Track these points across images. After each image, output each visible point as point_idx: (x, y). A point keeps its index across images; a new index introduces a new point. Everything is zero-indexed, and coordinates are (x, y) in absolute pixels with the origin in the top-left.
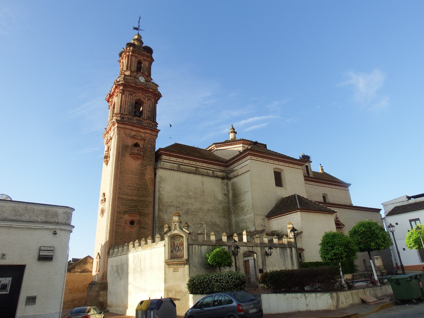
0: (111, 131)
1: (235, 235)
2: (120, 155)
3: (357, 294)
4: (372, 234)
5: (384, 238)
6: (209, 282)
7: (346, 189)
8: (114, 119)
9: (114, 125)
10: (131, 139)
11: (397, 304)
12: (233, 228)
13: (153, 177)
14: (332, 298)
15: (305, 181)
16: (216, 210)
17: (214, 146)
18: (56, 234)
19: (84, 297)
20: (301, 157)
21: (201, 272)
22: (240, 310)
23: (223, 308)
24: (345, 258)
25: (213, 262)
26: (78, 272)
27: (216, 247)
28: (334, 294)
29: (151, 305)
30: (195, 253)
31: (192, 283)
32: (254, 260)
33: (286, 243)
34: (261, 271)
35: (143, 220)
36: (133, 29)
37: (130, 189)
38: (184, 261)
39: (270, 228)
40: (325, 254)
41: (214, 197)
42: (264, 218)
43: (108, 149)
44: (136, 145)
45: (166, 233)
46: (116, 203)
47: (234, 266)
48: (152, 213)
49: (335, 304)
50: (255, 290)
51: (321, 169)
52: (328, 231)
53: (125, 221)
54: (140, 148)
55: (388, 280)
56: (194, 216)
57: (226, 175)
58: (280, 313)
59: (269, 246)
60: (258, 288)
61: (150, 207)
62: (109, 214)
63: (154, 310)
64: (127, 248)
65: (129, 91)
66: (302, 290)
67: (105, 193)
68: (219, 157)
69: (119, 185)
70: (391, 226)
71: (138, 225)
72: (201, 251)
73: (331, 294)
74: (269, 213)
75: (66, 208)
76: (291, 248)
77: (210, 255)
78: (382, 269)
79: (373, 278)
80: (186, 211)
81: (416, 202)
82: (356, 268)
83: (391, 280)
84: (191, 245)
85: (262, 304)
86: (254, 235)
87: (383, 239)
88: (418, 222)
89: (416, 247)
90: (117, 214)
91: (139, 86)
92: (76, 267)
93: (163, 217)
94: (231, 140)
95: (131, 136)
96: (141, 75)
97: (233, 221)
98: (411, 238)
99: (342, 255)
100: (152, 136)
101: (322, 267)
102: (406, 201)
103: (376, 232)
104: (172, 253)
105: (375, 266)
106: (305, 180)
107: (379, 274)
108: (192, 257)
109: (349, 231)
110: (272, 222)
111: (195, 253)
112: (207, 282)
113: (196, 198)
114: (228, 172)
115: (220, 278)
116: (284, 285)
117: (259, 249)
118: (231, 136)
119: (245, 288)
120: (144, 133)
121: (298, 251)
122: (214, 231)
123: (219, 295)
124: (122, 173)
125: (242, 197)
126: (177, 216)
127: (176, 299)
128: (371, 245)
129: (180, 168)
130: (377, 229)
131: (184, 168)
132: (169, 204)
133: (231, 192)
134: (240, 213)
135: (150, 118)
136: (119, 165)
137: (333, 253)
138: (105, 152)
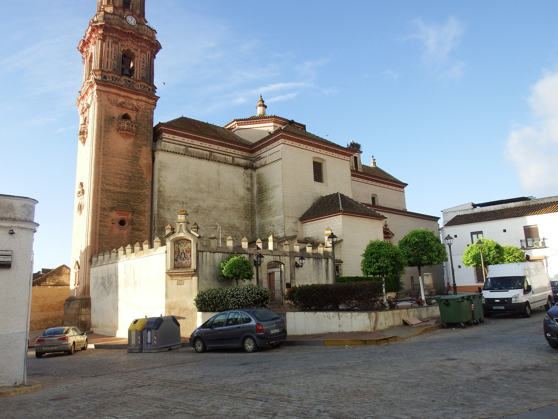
0: (87, 95)
1: (259, 240)
2: (102, 130)
3: (400, 314)
4: (426, 246)
5: (439, 251)
6: (222, 297)
7: (402, 190)
8: (91, 78)
9: (92, 86)
10: (118, 108)
11: (442, 327)
12: (257, 232)
13: (151, 162)
14: (370, 318)
15: (352, 177)
16: (235, 208)
17: (235, 124)
18: (13, 233)
19: (60, 316)
20: (349, 145)
21: (212, 285)
22: (259, 329)
23: (239, 328)
24: (391, 272)
25: (228, 274)
26: (51, 285)
27: (234, 255)
28: (373, 314)
29: (148, 324)
30: (206, 262)
31: (201, 298)
32: (281, 272)
33: (322, 252)
34: (288, 285)
35: (137, 219)
37: (119, 178)
38: (191, 272)
39: (304, 234)
40: (367, 268)
41: (234, 191)
42: (297, 221)
43: (85, 121)
44: (126, 117)
45: (168, 236)
46: (99, 197)
47: (255, 279)
48: (150, 210)
49: (373, 325)
50: (280, 307)
51: (373, 162)
52: (374, 239)
53: (113, 220)
54: (131, 122)
55: (437, 300)
56: (205, 216)
57: (250, 163)
58: (308, 334)
59: (301, 256)
60: (283, 305)
61: (147, 202)
62: (90, 210)
63: (152, 330)
64: (115, 255)
66: (336, 309)
67: (82, 183)
68: (241, 139)
69: (102, 172)
70: (449, 237)
71: (130, 226)
72: (214, 259)
73: (370, 314)
74: (303, 216)
75: (25, 199)
76: (328, 259)
77: (225, 264)
78: (431, 287)
79: (420, 297)
80: (195, 209)
81: (482, 212)
82: (402, 286)
83: (441, 300)
84: (200, 251)
85: (286, 324)
86: (282, 241)
87: (437, 252)
88: (480, 235)
89: (473, 264)
90: (101, 210)
91: (128, 30)
92: (48, 279)
93: (164, 216)
94: (259, 116)
95: (118, 103)
96: (130, 13)
97: (257, 224)
98: (470, 254)
99: (387, 269)
100: (148, 104)
101: (363, 282)
102: (470, 209)
103: (431, 244)
104: (176, 262)
105: (423, 284)
106: (352, 175)
107: (427, 293)
108: (202, 266)
109: (399, 241)
110: (307, 227)
111: (206, 262)
112: (220, 298)
113: (209, 192)
114: (253, 159)
115: (237, 293)
116: (315, 301)
117: (288, 259)
118: (259, 111)
119: (268, 305)
120: (136, 100)
121: (336, 263)
122: (232, 235)
123: (234, 313)
124: (106, 156)
125: (270, 193)
126: (183, 214)
127: (180, 318)
128: (422, 258)
129: (187, 151)
130: (433, 240)
131: (194, 151)
132: (172, 199)
133: (256, 186)
134: (267, 213)
135: (144, 78)
136: (102, 144)
137: (377, 266)
138: (80, 125)
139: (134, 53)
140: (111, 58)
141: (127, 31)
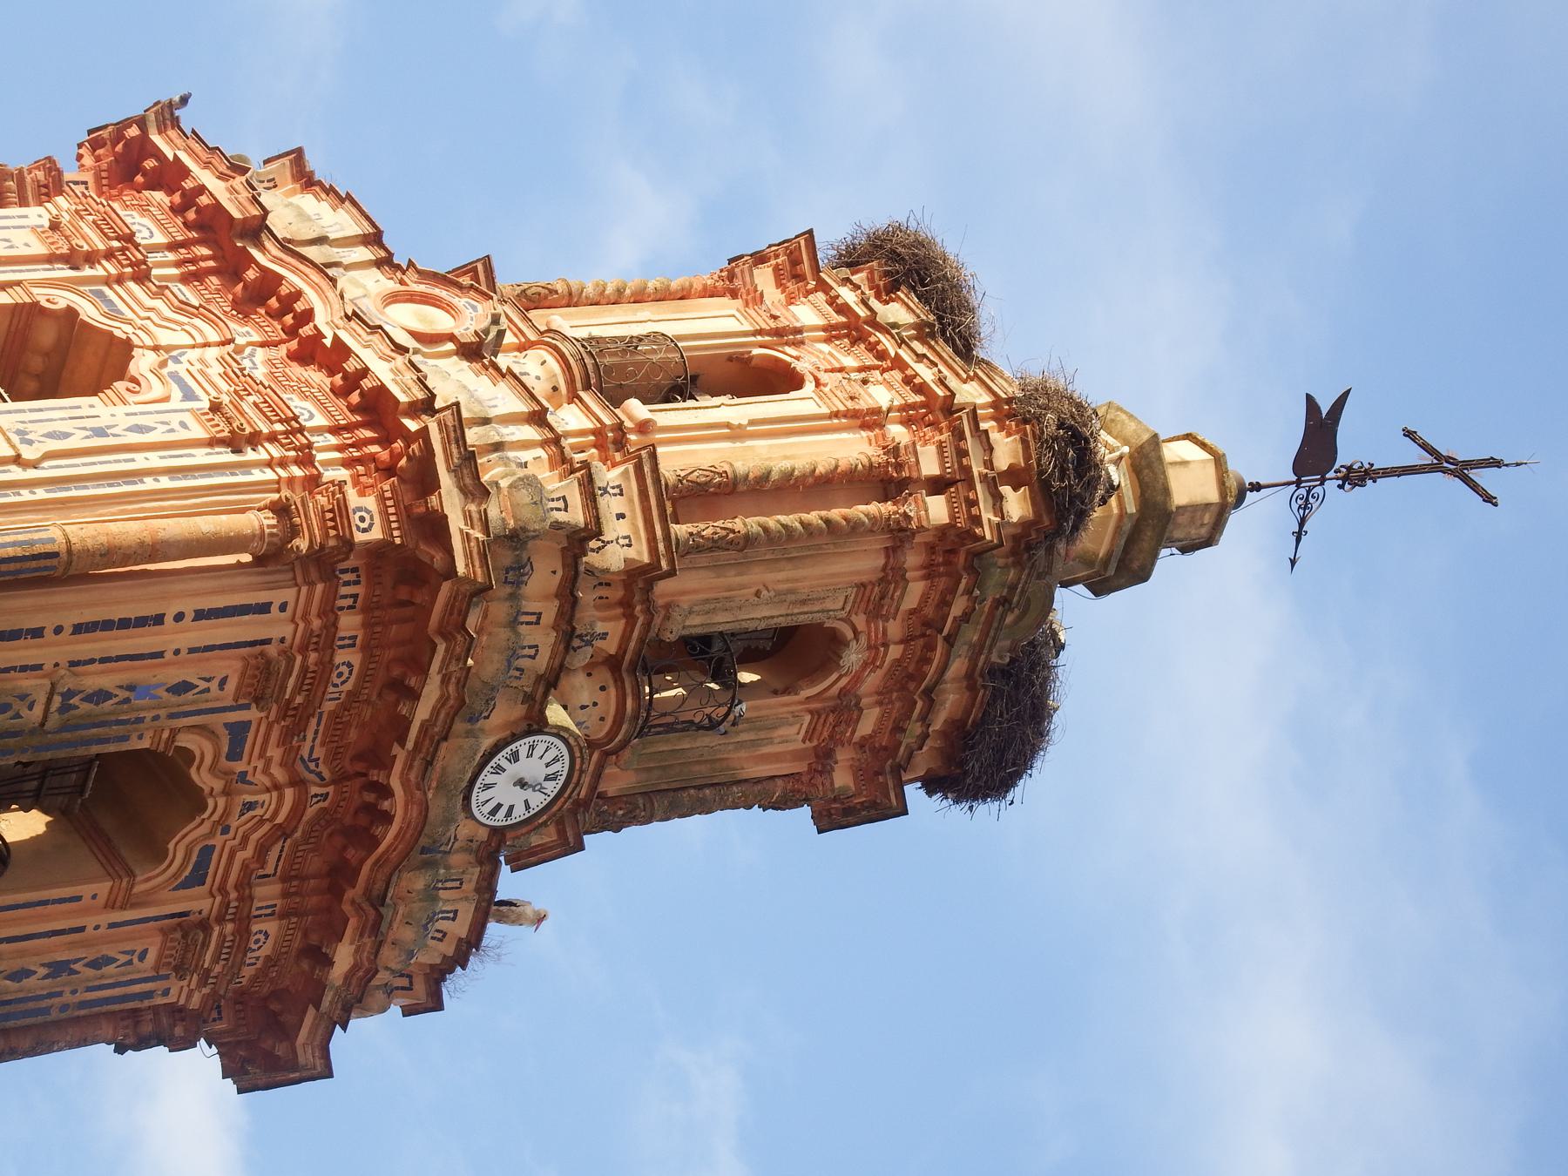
36: (1309, 398)
65: (326, 640)
91: (416, 788)
139: (158, 854)
140: (73, 664)
141: (405, 783)
